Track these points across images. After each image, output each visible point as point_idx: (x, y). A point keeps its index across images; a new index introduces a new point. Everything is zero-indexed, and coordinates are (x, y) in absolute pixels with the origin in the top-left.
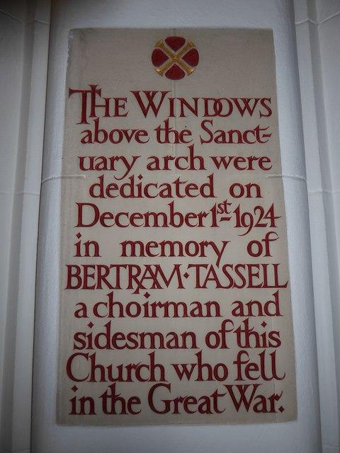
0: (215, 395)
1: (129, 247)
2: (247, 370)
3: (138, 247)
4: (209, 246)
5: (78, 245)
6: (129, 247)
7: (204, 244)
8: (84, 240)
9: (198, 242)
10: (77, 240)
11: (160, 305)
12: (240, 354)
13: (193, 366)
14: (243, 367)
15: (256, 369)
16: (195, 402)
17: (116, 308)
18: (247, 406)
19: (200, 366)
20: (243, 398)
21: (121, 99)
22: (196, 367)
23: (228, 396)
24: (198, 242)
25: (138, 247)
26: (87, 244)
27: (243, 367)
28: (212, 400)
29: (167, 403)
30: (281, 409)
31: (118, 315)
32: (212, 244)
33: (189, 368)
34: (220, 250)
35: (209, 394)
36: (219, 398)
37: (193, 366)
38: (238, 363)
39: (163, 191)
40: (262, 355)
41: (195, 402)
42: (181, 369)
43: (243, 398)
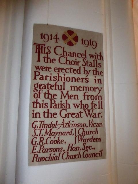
0: (80, 112)
1: (73, 88)
2: (94, 106)
3: (76, 88)
4: (97, 89)
5: (33, 114)
6: (73, 88)
7: (95, 88)
8: (35, 112)
9: (94, 87)
10: (33, 112)
11: (70, 114)
12: (92, 102)
13: (79, 104)
14: (93, 105)
15: (84, 55)
16: (74, 114)
17: (50, 115)
18: (91, 116)
19: (81, 104)
20: (89, 113)
21: (41, 44)
22: (80, 105)
23: (84, 113)
24: (94, 87)
25: (76, 88)
26: (36, 114)
27: (93, 105)
28: (79, 114)
29: (66, 115)
30: (102, 126)
31: (50, 117)
32: (98, 88)
33: (78, 105)
34: (100, 90)
35: (78, 112)
36: (81, 113)
37: (79, 104)
38: (92, 104)
39: (97, 125)
40: (99, 102)
41: (74, 114)
42: (75, 105)
43: (89, 113)
